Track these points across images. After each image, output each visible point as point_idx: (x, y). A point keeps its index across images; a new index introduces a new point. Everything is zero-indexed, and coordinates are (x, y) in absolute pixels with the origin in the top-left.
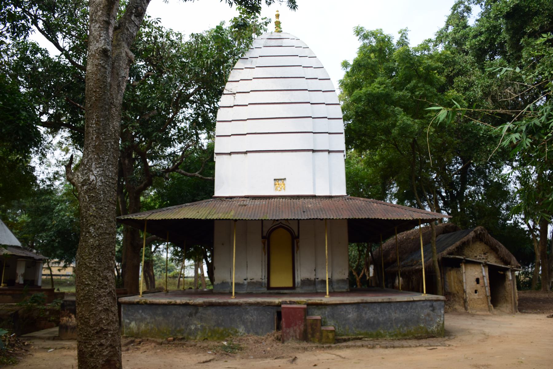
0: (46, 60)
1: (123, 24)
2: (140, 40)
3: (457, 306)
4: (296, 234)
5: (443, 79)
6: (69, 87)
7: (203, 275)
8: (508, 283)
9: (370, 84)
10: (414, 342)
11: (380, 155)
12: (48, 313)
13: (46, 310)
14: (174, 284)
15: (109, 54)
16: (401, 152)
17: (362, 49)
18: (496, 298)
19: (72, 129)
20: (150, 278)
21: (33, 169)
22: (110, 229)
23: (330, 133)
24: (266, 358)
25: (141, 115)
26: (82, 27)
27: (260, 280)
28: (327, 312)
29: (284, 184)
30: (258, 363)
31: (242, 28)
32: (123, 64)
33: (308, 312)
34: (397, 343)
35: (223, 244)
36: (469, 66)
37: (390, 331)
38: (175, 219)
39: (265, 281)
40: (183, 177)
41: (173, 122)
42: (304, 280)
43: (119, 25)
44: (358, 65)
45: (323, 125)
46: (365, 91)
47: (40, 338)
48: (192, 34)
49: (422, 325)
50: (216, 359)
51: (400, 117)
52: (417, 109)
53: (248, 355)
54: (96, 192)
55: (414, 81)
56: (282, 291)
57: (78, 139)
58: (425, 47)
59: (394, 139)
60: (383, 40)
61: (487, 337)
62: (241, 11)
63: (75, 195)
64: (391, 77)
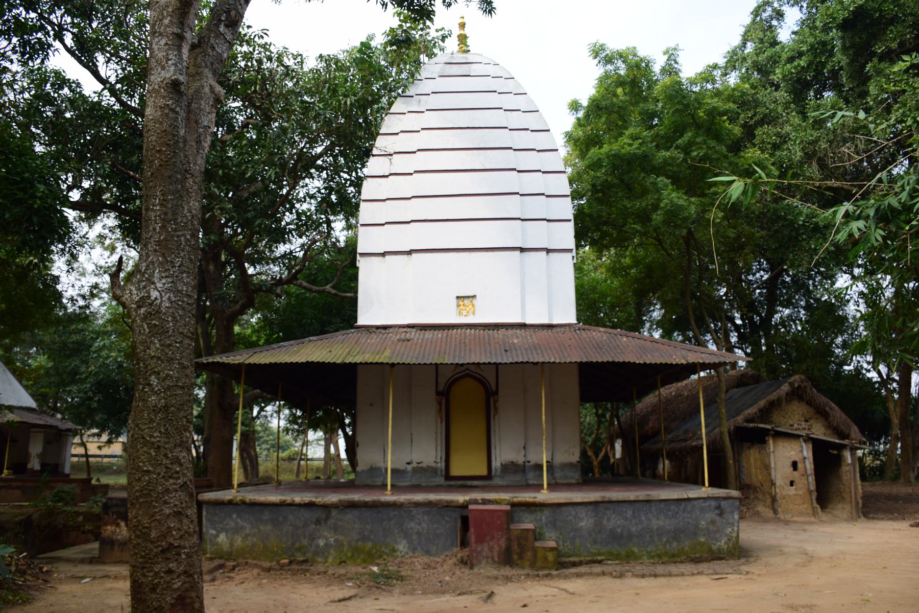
0: (78, 100)
1: (206, 40)
2: (233, 66)
3: (760, 508)
4: (494, 388)
5: (737, 130)
6: (116, 143)
7: (339, 455)
8: (845, 468)
9: (616, 138)
10: (687, 568)
11: (633, 257)
12: (81, 518)
13: (78, 514)
14: (291, 471)
15: (183, 88)
16: (666, 252)
17: (602, 80)
18: (825, 494)
19: (121, 214)
21: (56, 279)
22: (183, 380)
23: (549, 221)
24: (443, 593)
25: (236, 189)
27: (434, 465)
29: (473, 305)
30: (429, 601)
31: (405, 47)
32: (206, 105)
33: (512, 517)
34: (660, 569)
35: (371, 405)
36: (780, 109)
37: (649, 549)
38: (292, 363)
39: (442, 465)
41: (288, 202)
42: (506, 465)
43: (199, 41)
44: (596, 108)
45: (536, 208)
47: (68, 560)
48: (321, 56)
49: (702, 539)
50: (361, 595)
51: (665, 193)
52: (694, 180)
53: (414, 589)
54: (160, 318)
55: (690, 134)
56: (469, 483)
57: (132, 229)
58: (707, 76)
60: (638, 66)
61: (810, 559)
63: (125, 322)
64: (652, 127)
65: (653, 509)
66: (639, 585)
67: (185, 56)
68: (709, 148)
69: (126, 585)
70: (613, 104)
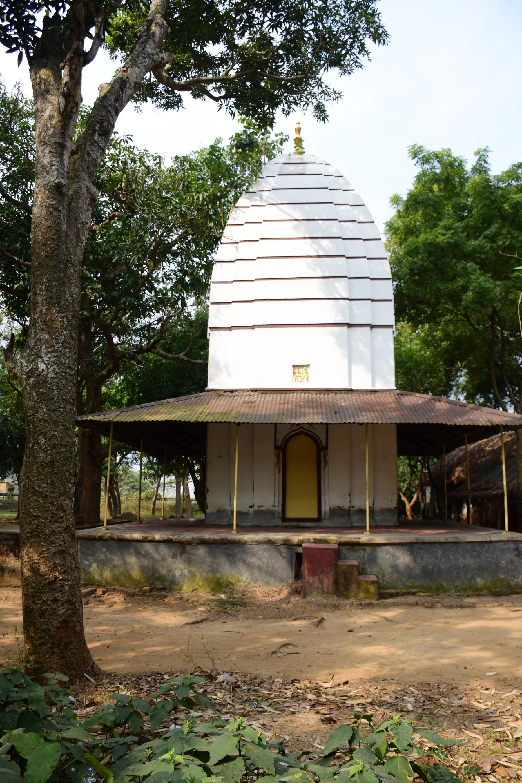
1: (83, 147)
2: (102, 167)
4: (324, 443)
7: (189, 496)
9: (432, 229)
11: (443, 330)
14: (148, 509)
15: (64, 190)
16: (474, 327)
17: (419, 178)
20: (115, 503)
22: (66, 440)
23: (373, 300)
24: (281, 618)
25: (104, 271)
26: (19, 147)
28: (366, 556)
29: (307, 373)
31: (246, 146)
32: (84, 204)
35: (220, 457)
37: (456, 584)
39: (279, 509)
40: (162, 360)
41: (148, 282)
43: (77, 148)
44: (414, 202)
45: (363, 289)
46: (424, 239)
48: (177, 158)
49: (502, 576)
50: (211, 618)
53: (256, 615)
54: (47, 387)
55: (497, 226)
56: (302, 524)
59: (464, 309)
60: (451, 165)
62: (245, 124)
63: (10, 383)
64: (462, 218)
65: (460, 550)
66: (447, 614)
67: (66, 163)
68: (513, 237)
70: (428, 199)
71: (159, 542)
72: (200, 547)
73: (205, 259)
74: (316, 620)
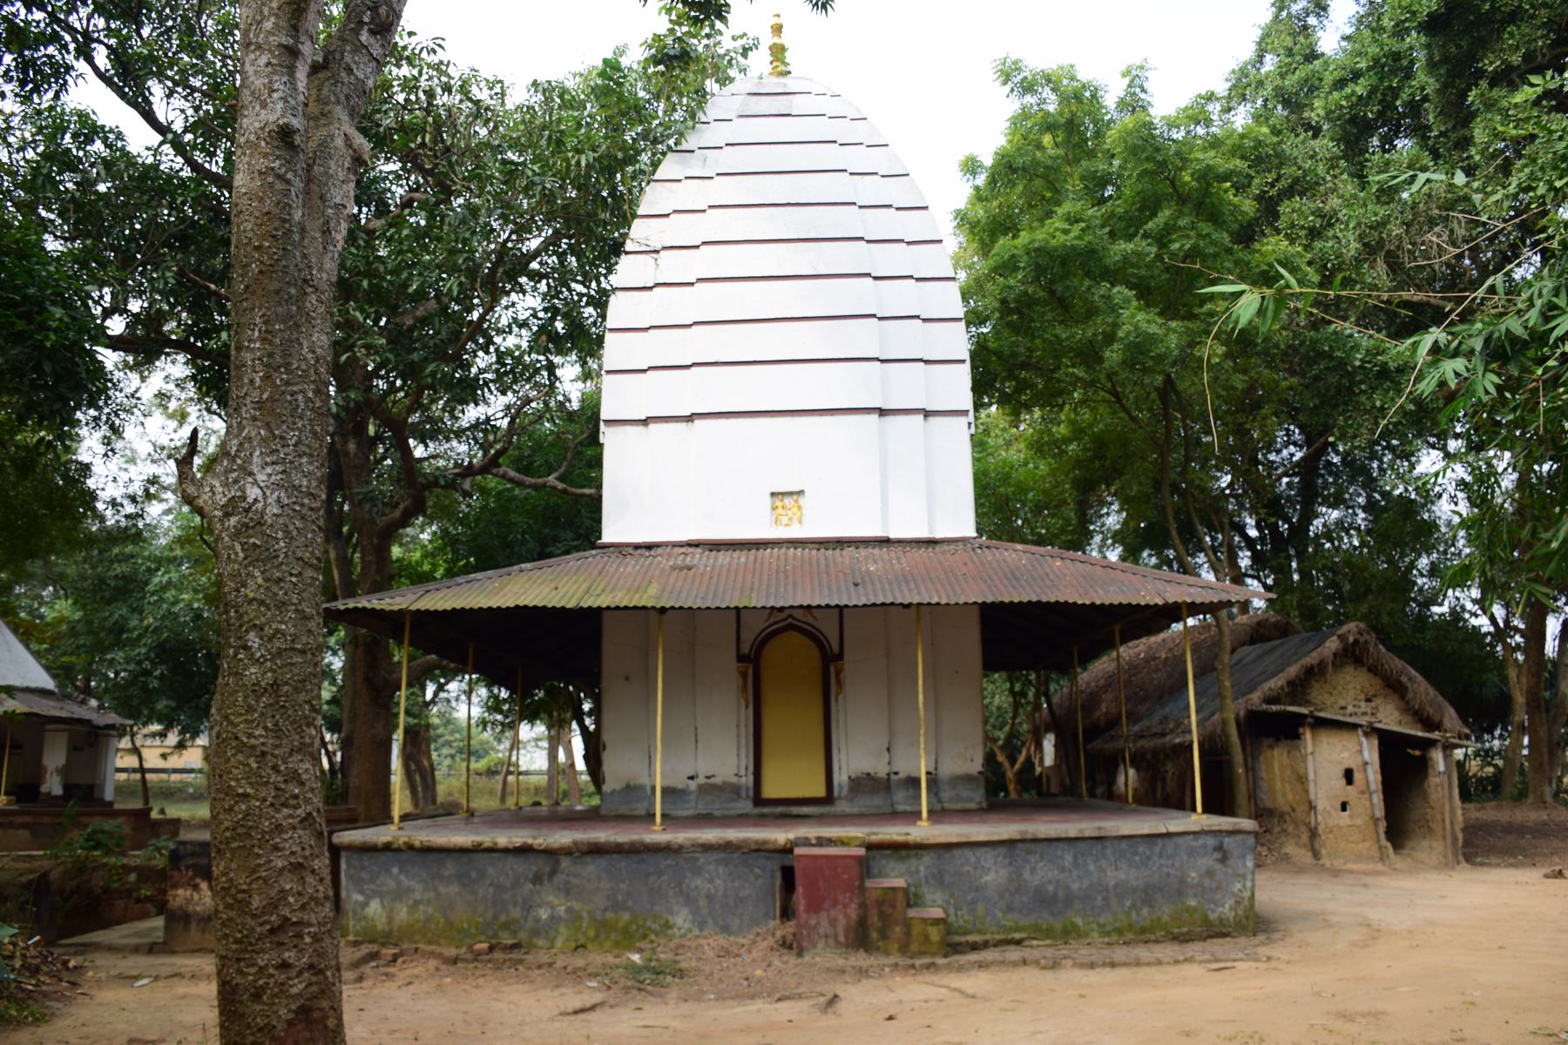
0: (118, 162)
1: (337, 56)
3: (1290, 849)
4: (836, 648)
5: (1248, 206)
6: (185, 236)
7: (572, 765)
8: (1433, 780)
9: (1042, 221)
11: (1072, 423)
12: (133, 877)
13: (127, 869)
14: (491, 793)
15: (298, 140)
16: (1128, 413)
18: (1399, 823)
19: (195, 355)
20: (421, 775)
21: (86, 469)
23: (927, 362)
24: (752, 997)
25: (393, 311)
27: (734, 780)
29: (800, 508)
30: (728, 1012)
31: (675, 62)
32: (338, 168)
33: (868, 868)
34: (1121, 953)
35: (627, 679)
36: (1321, 170)
37: (1102, 920)
39: (749, 780)
41: (481, 333)
43: (326, 59)
44: (1007, 169)
45: (907, 340)
47: (112, 949)
48: (535, 84)
49: (1192, 903)
50: (611, 1001)
51: (1126, 313)
52: (1175, 292)
53: (702, 992)
55: (1167, 213)
56: (795, 810)
57: (214, 382)
59: (1109, 377)
60: (1077, 96)
61: (1374, 934)
64: (1102, 201)
65: (1108, 852)
69: (211, 989)
71: (506, 851)
72: (588, 859)
73: (594, 285)
74: (822, 999)
